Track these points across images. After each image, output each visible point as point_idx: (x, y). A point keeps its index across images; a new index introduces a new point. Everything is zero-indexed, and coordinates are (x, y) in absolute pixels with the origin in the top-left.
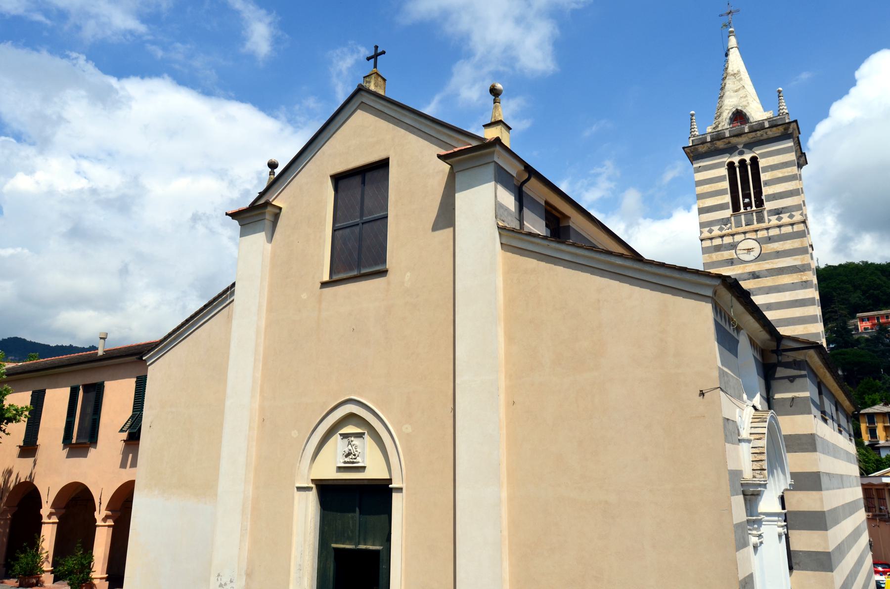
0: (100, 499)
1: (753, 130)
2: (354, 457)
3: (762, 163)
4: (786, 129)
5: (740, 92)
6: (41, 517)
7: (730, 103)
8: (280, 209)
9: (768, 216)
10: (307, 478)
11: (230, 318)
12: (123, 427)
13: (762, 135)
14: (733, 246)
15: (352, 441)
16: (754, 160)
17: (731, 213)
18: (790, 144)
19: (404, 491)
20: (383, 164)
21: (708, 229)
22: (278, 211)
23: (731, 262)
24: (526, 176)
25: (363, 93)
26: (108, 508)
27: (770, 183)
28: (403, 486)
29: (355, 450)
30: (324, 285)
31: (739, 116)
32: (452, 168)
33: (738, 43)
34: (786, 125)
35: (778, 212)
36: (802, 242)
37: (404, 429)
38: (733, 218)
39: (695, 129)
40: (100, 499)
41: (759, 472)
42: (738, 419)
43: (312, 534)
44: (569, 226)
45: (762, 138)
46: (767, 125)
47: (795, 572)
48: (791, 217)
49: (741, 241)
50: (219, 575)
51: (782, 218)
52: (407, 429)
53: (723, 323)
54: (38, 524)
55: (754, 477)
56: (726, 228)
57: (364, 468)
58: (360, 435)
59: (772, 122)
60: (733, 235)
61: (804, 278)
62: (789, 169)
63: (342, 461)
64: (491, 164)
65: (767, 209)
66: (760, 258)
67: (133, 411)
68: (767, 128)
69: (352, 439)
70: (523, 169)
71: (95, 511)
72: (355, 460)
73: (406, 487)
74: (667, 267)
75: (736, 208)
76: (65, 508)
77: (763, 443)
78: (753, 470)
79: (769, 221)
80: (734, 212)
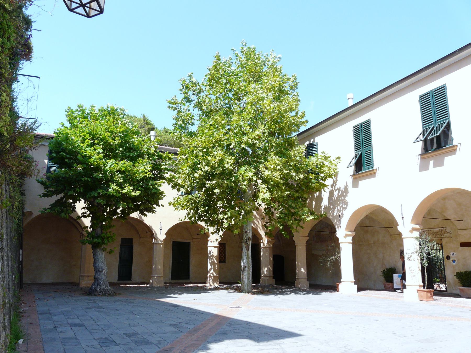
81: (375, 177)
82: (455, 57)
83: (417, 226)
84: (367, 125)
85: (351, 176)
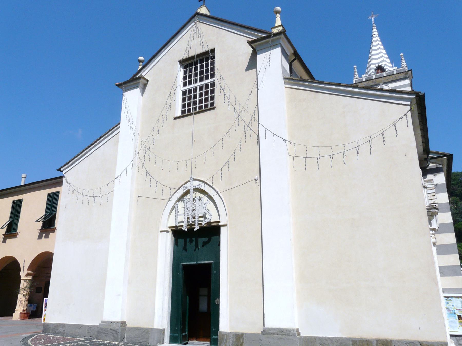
0: (24, 264)
8: (148, 81)
11: (117, 143)
22: (146, 82)
24: (294, 58)
26: (29, 269)
31: (380, 69)
39: (357, 75)
40: (24, 264)
64: (278, 45)
67: (45, 213)
70: (293, 52)
81: (16, 238)
82: (47, 182)
83: (31, 272)
84: (20, 202)
85: (3, 235)
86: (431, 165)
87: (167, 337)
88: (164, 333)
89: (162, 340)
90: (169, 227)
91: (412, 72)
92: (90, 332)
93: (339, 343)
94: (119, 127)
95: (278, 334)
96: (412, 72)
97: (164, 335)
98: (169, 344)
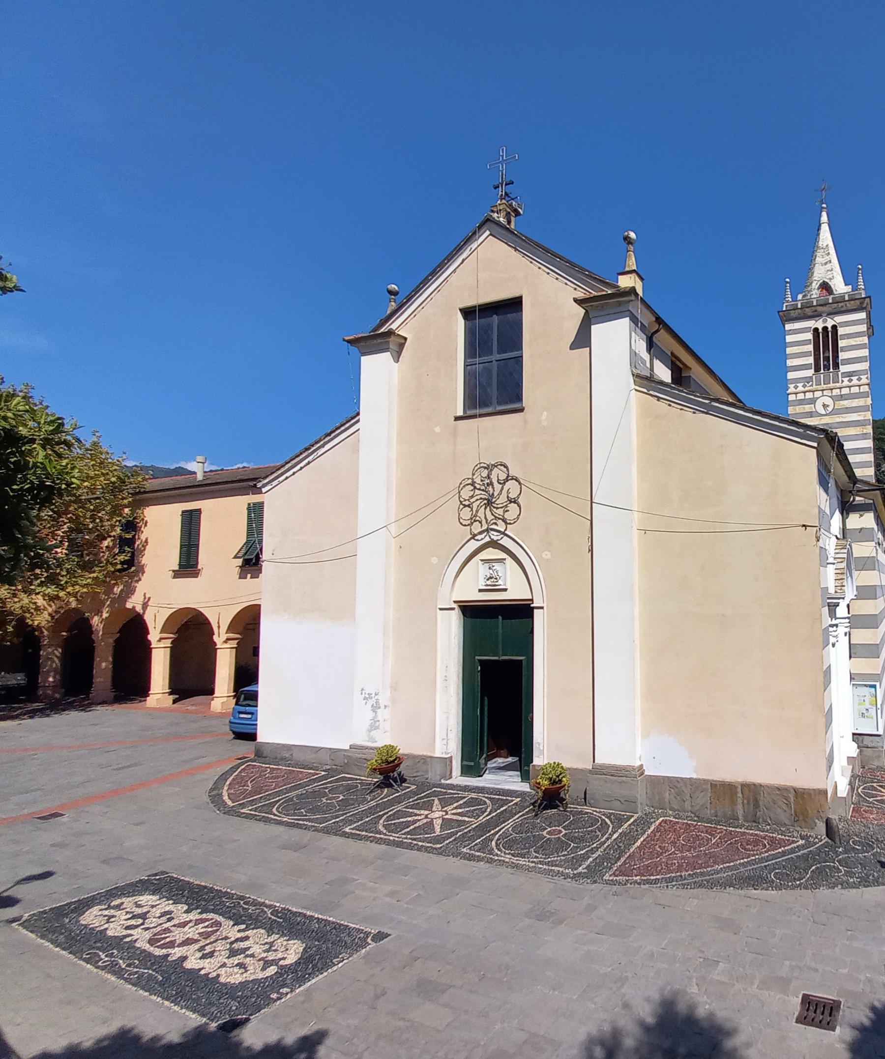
0: (218, 623)
1: (835, 302)
2: (495, 580)
3: (841, 331)
4: (862, 303)
5: (827, 266)
6: (150, 643)
7: (819, 274)
8: (406, 339)
9: (842, 377)
10: (450, 600)
12: (237, 554)
13: (842, 307)
14: (813, 401)
15: (493, 566)
16: (834, 328)
17: (813, 373)
18: (862, 315)
19: (545, 608)
20: (515, 304)
21: (794, 385)
22: (403, 341)
23: (811, 414)
25: (489, 223)
27: (844, 349)
28: (545, 605)
29: (496, 574)
30: (457, 419)
31: (826, 287)
32: (587, 312)
33: (829, 219)
34: (862, 300)
35: (850, 375)
36: (866, 401)
37: (544, 556)
38: (814, 377)
41: (839, 588)
42: (827, 548)
43: (457, 649)
44: (690, 376)
45: (842, 309)
46: (847, 298)
47: (852, 659)
48: (859, 379)
49: (819, 397)
50: (362, 690)
51: (852, 380)
52: (547, 555)
53: (823, 472)
54: (146, 650)
55: (836, 592)
56: (808, 385)
57: (505, 590)
58: (501, 561)
59: (850, 296)
60: (813, 391)
61: (865, 431)
62: (861, 339)
63: (484, 584)
65: (842, 371)
66: (835, 412)
67: (247, 538)
68: (847, 301)
69: (494, 564)
71: (214, 634)
72: (496, 583)
73: (547, 606)
74: (782, 420)
75: (817, 370)
76: (176, 633)
77: (844, 565)
78: (836, 586)
79: (843, 381)
80: (815, 371)
86: (857, 498)
87: (457, 768)
88: (451, 762)
89: (449, 773)
90: (455, 602)
91: (870, 300)
92: (333, 758)
93: (694, 786)
94: (358, 421)
95: (612, 775)
96: (870, 300)
97: (451, 766)
98: (461, 776)
